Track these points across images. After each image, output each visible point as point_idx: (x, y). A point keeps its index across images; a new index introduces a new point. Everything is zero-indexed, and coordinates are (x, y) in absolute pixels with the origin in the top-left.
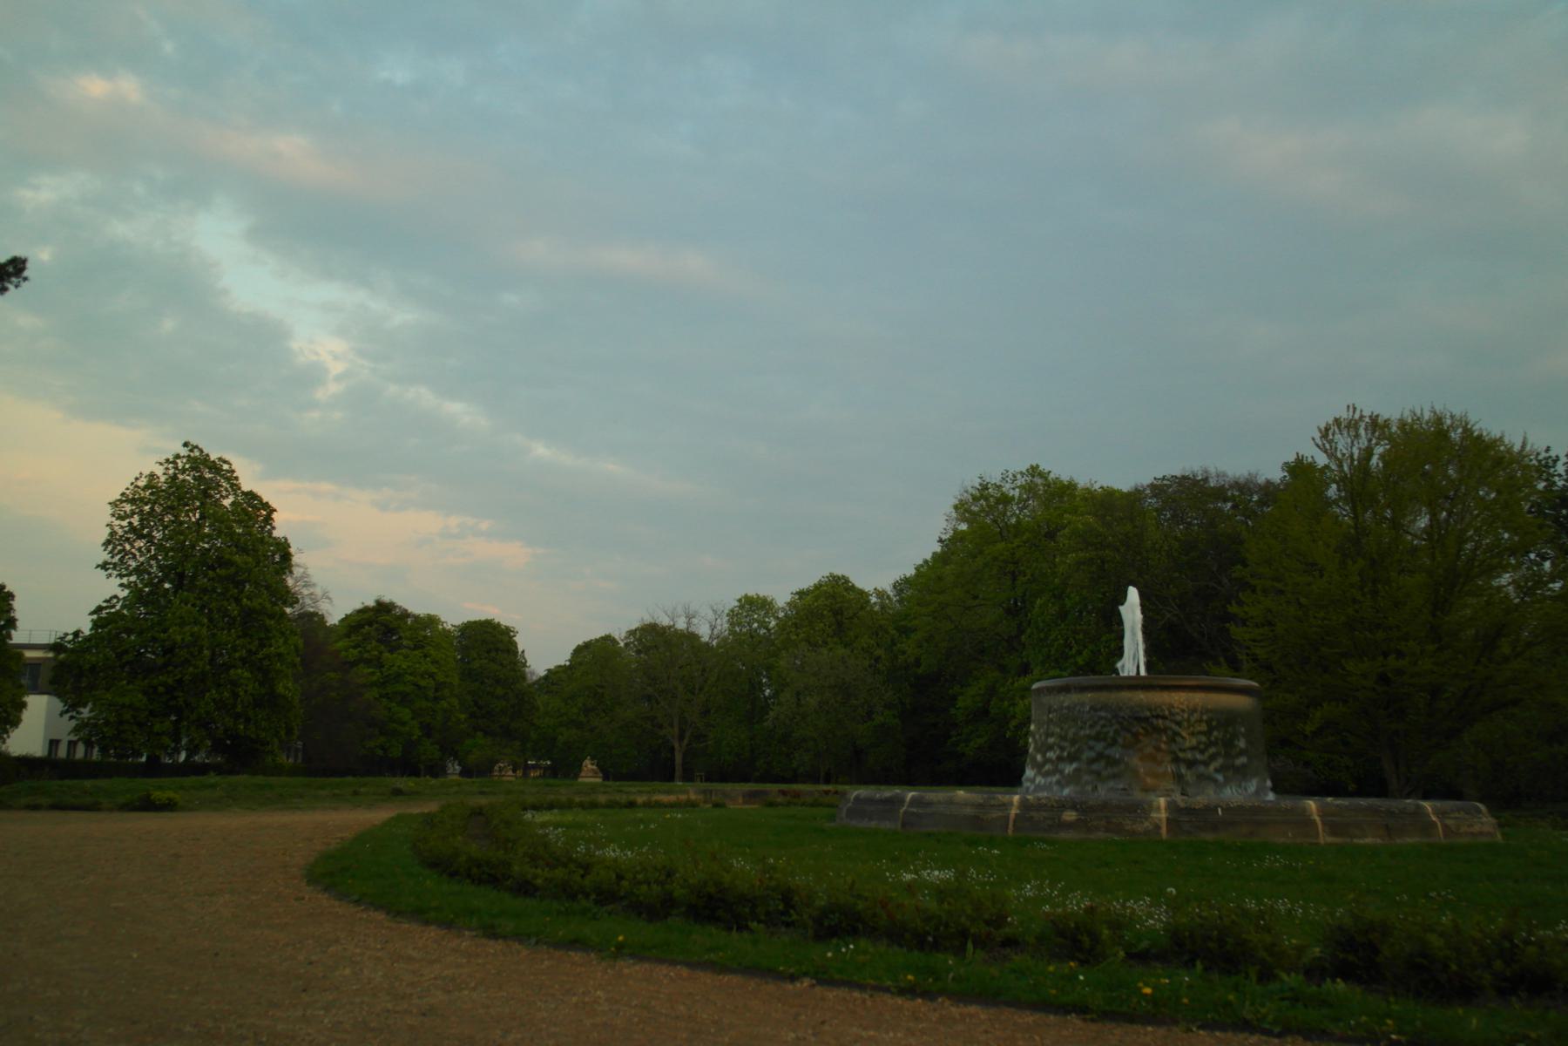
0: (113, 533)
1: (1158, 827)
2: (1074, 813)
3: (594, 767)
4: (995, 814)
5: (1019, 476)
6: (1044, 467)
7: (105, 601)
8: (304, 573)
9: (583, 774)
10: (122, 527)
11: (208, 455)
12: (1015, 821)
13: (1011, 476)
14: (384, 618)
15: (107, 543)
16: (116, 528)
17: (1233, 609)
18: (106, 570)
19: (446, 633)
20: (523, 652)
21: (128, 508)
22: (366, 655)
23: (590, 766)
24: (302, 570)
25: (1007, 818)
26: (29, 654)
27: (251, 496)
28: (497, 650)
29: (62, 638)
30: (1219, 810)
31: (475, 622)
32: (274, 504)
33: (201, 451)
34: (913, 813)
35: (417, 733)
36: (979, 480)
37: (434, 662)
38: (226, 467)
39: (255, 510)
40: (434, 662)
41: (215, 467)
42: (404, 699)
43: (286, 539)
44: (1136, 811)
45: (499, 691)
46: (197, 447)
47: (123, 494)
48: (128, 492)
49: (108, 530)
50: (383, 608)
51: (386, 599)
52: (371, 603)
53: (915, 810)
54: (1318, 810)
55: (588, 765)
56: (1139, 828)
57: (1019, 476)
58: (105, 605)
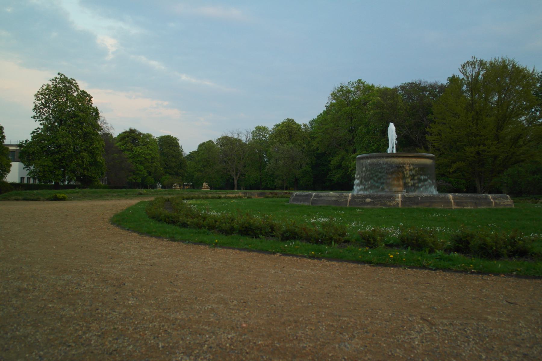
0: (36, 106)
1: (398, 204)
2: (370, 199)
3: (207, 185)
4: (343, 200)
5: (354, 83)
6: (363, 80)
7: (35, 130)
8: (104, 119)
9: (203, 188)
10: (39, 103)
11: (67, 78)
12: (350, 202)
13: (351, 83)
14: (132, 135)
15: (34, 109)
16: (37, 104)
17: (428, 129)
18: (35, 118)
19: (154, 140)
20: (181, 146)
21: (40, 97)
22: (127, 148)
23: (205, 185)
24: (103, 118)
25: (347, 201)
26: (11, 148)
27: (83, 92)
28: (172, 146)
29: (21, 143)
30: (443, 206)
31: (164, 136)
32: (91, 95)
33: (65, 76)
34: (315, 200)
35: (146, 174)
36: (341, 85)
37: (151, 150)
38: (74, 82)
39: (85, 97)
40: (151, 150)
41: (70, 82)
42: (141, 163)
43: (97, 107)
44: (391, 199)
45: (174, 160)
46: (63, 75)
47: (38, 92)
48: (40, 91)
49: (34, 105)
50: (132, 131)
51: (133, 128)
52: (128, 130)
53: (316, 199)
54: (453, 198)
55: (205, 184)
56: (392, 204)
57: (354, 83)
58: (35, 131)
